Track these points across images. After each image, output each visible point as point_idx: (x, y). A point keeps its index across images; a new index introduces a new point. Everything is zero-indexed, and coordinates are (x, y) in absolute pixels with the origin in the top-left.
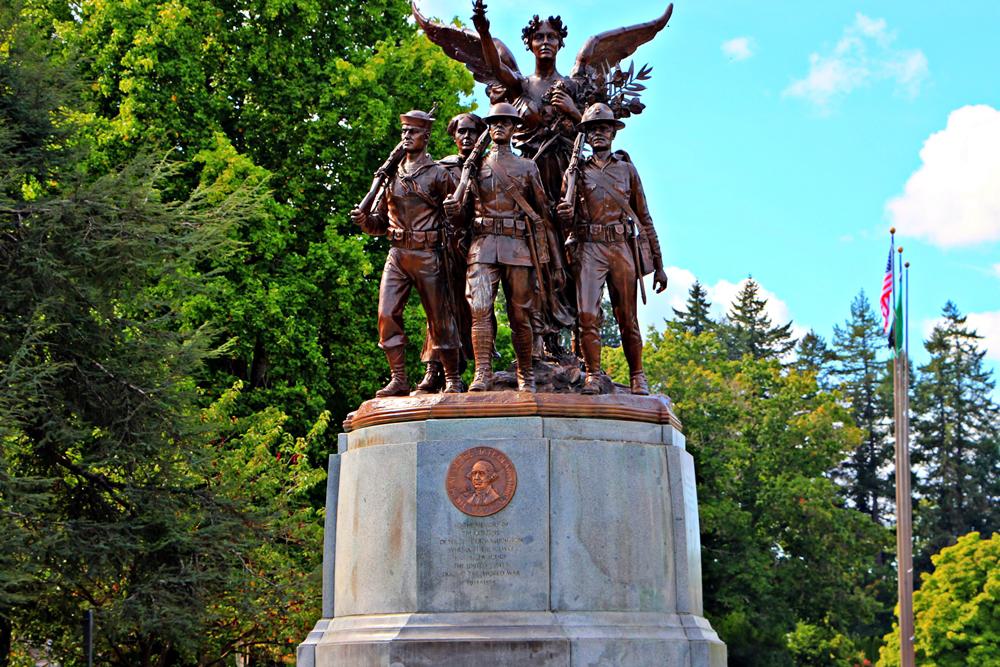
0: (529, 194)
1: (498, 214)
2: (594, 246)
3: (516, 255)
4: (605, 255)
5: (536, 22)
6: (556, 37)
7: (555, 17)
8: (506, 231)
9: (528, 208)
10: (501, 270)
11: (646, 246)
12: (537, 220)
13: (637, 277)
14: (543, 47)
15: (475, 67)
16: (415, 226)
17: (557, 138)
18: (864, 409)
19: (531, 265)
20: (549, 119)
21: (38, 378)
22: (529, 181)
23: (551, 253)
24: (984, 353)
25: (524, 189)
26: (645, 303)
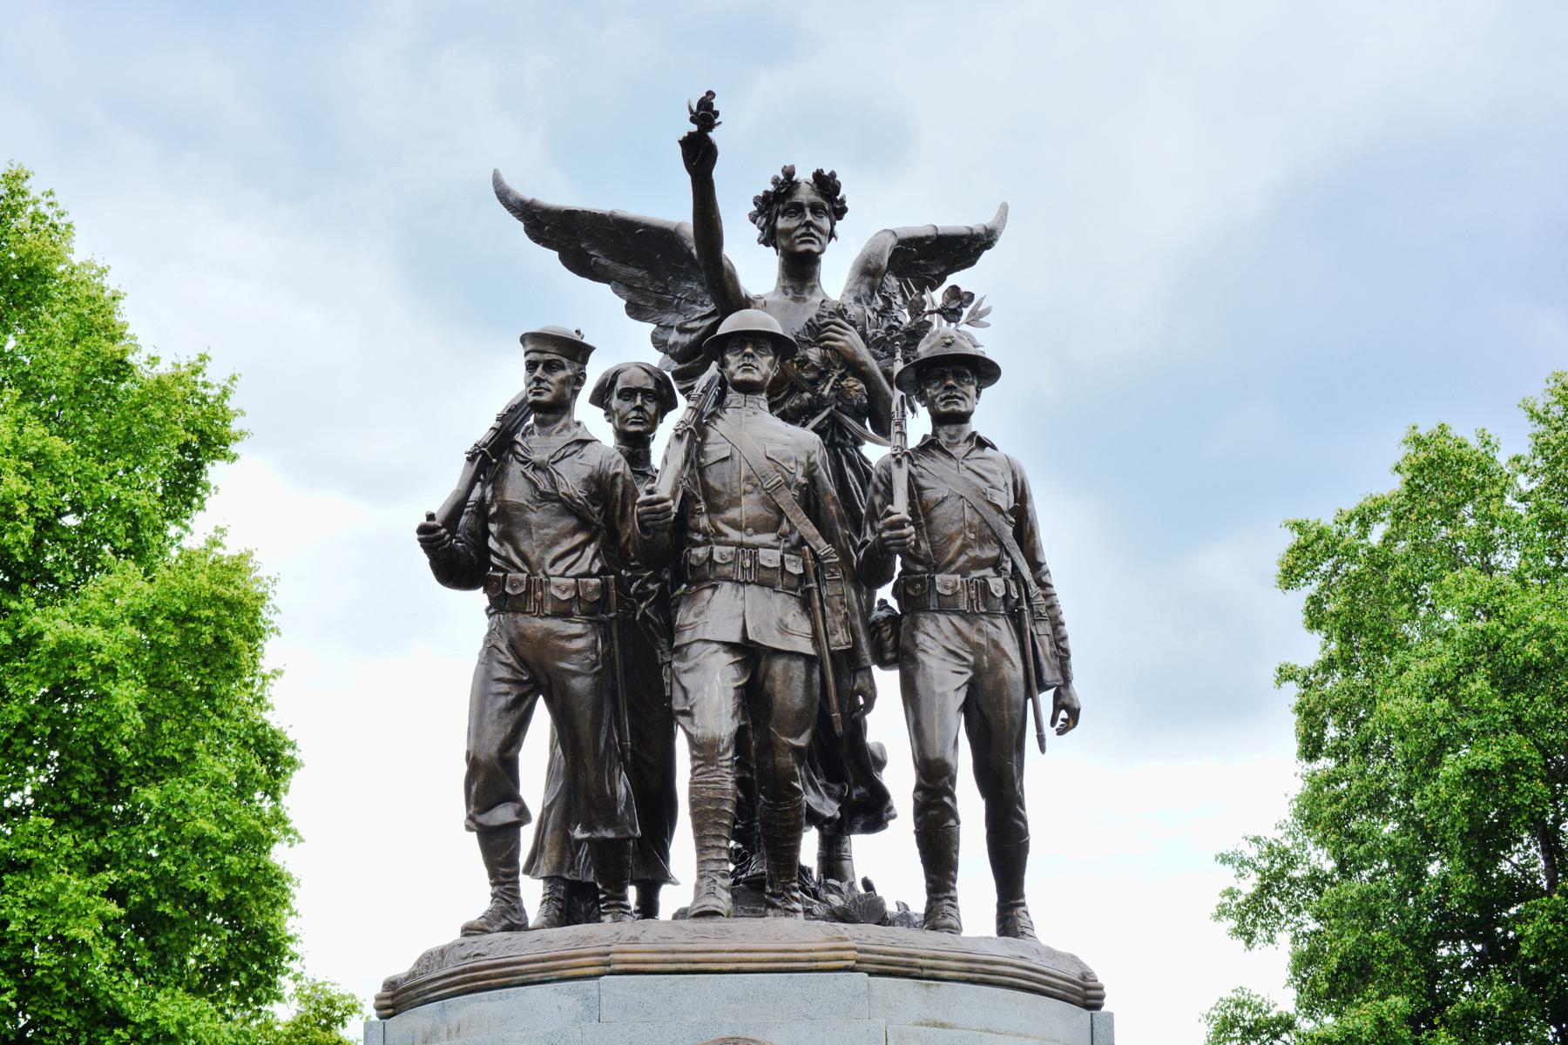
0: (810, 499)
1: (746, 539)
2: (942, 618)
3: (784, 629)
4: (966, 640)
5: (787, 184)
6: (827, 213)
7: (826, 173)
8: (765, 574)
9: (808, 529)
10: (749, 654)
11: (1044, 628)
12: (827, 557)
13: (1029, 693)
14: (634, 414)
15: (630, 288)
16: (552, 564)
18: (106, 808)
19: (811, 652)
20: (811, 375)
22: (810, 473)
23: (853, 631)
24: (1225, 859)
26: (1043, 749)
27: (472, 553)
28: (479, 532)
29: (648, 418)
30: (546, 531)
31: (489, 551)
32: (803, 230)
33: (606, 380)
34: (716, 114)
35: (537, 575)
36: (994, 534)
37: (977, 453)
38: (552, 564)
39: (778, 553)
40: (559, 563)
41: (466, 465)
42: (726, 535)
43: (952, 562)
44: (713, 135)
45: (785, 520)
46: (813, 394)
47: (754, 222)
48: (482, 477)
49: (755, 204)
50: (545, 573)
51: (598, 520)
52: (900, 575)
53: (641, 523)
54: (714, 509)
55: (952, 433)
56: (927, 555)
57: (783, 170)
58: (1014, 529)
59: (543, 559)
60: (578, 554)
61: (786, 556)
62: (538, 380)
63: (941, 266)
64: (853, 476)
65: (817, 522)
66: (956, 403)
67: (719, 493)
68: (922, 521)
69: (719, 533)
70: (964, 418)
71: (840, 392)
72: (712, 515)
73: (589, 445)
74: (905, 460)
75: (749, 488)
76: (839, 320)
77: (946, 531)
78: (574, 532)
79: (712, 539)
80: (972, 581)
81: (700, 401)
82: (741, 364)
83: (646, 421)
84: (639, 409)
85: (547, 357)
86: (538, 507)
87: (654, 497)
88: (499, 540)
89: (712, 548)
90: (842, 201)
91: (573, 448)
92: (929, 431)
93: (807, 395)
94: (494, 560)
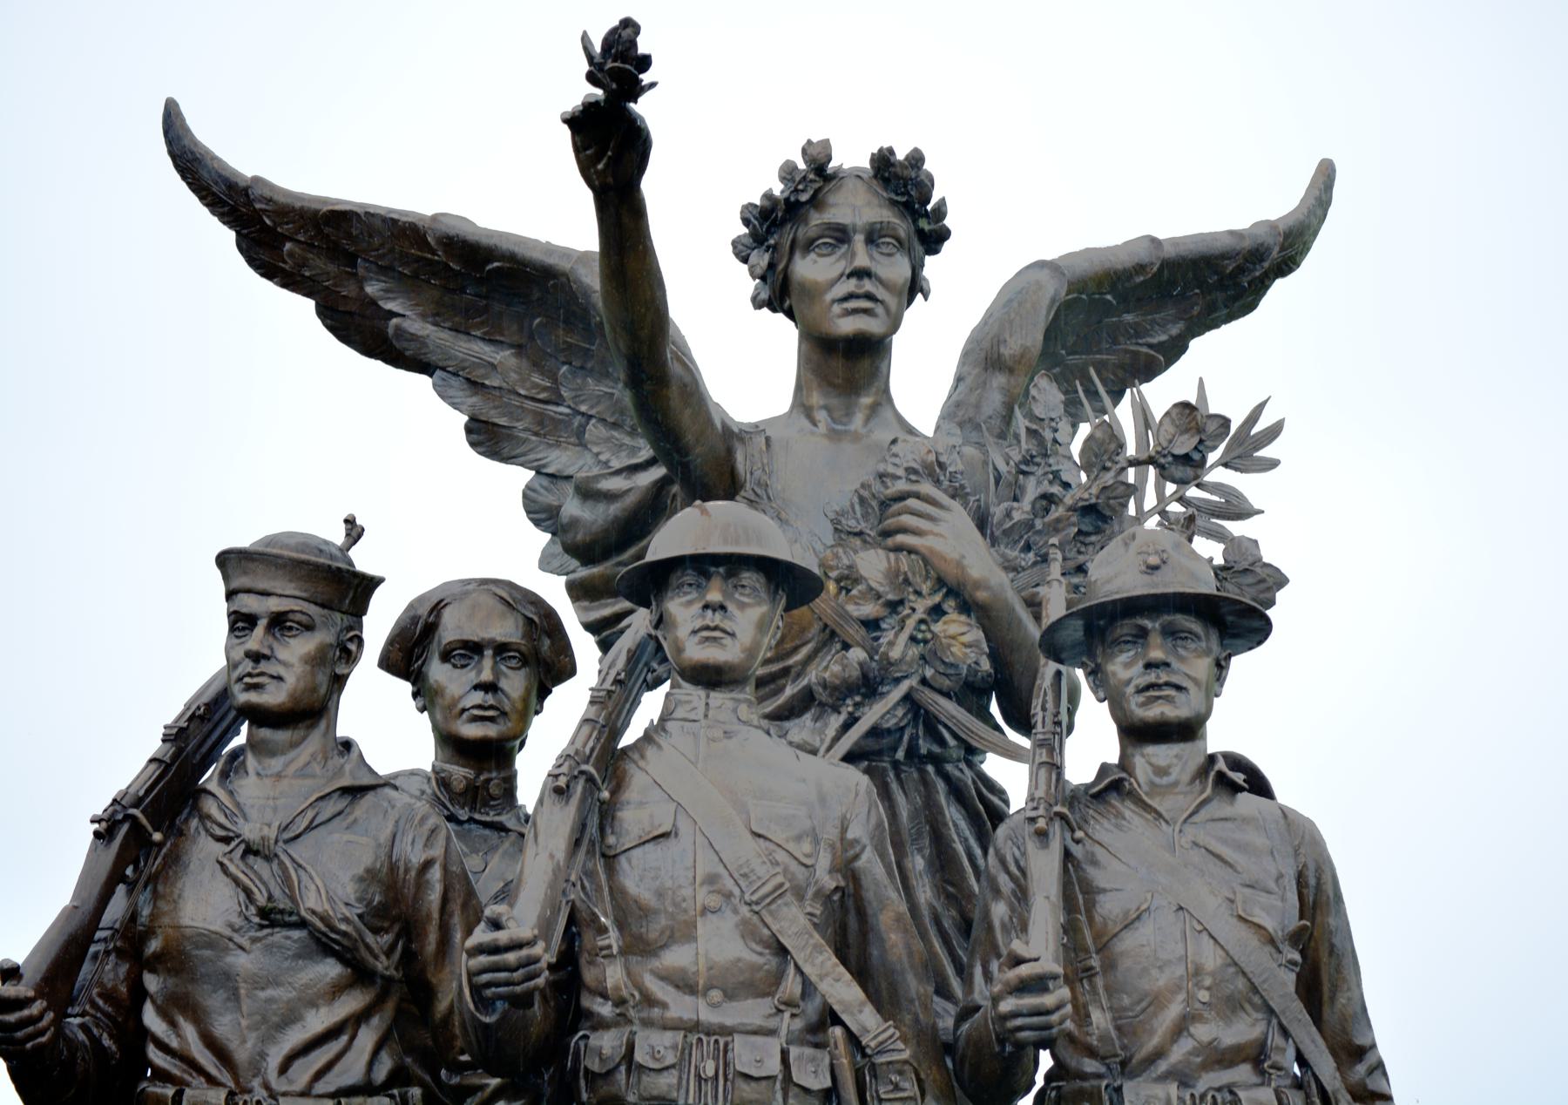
1: (707, 1016)
7: (901, 155)
9: (842, 990)
15: (475, 385)
17: (908, 698)
20: (869, 609)
21: (1109, 444)
22: (847, 869)
25: (825, 897)
27: (107, 1042)
28: (123, 989)
29: (507, 708)
30: (270, 992)
31: (145, 1034)
32: (851, 285)
33: (415, 620)
34: (645, 63)
35: (250, 1091)
36: (1255, 990)
37: (1220, 807)
38: (284, 1068)
39: (774, 1046)
40: (298, 1064)
41: (93, 850)
42: (664, 1006)
43: (1158, 1054)
44: (642, 107)
45: (791, 970)
46: (871, 652)
47: (745, 260)
48: (129, 871)
49: (746, 222)
50: (267, 1086)
51: (382, 965)
52: (1049, 1077)
53: (476, 990)
54: (638, 947)
55: (1162, 763)
56: (1104, 1038)
57: (804, 151)
58: (1298, 975)
59: (263, 1055)
60: (344, 1039)
61: (794, 1052)
62: (256, 657)
63: (1174, 322)
64: (963, 824)
65: (862, 974)
66: (1168, 699)
67: (646, 912)
68: (1095, 962)
69: (649, 1001)
70: (1189, 730)
71: (931, 652)
72: (634, 959)
73: (370, 797)
74: (1057, 828)
75: (714, 901)
76: (926, 488)
77: (1145, 985)
78: (337, 990)
79: (632, 1013)
80: (1203, 1097)
81: (610, 705)
82: (698, 624)
83: (504, 714)
84: (490, 687)
85: (274, 605)
86: (254, 940)
87: (502, 937)
88: (163, 1013)
89: (633, 1033)
90: (940, 212)
91: (330, 808)
92: (1113, 757)
93: (857, 654)
94: (154, 1054)
